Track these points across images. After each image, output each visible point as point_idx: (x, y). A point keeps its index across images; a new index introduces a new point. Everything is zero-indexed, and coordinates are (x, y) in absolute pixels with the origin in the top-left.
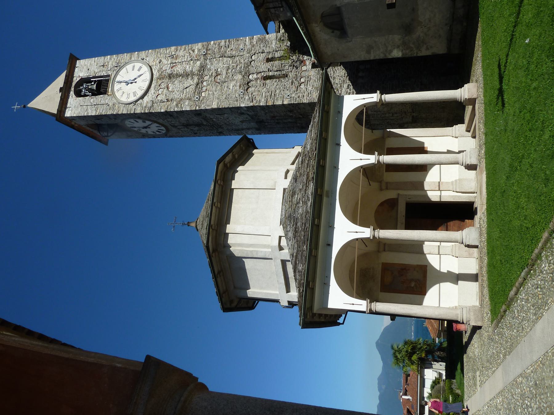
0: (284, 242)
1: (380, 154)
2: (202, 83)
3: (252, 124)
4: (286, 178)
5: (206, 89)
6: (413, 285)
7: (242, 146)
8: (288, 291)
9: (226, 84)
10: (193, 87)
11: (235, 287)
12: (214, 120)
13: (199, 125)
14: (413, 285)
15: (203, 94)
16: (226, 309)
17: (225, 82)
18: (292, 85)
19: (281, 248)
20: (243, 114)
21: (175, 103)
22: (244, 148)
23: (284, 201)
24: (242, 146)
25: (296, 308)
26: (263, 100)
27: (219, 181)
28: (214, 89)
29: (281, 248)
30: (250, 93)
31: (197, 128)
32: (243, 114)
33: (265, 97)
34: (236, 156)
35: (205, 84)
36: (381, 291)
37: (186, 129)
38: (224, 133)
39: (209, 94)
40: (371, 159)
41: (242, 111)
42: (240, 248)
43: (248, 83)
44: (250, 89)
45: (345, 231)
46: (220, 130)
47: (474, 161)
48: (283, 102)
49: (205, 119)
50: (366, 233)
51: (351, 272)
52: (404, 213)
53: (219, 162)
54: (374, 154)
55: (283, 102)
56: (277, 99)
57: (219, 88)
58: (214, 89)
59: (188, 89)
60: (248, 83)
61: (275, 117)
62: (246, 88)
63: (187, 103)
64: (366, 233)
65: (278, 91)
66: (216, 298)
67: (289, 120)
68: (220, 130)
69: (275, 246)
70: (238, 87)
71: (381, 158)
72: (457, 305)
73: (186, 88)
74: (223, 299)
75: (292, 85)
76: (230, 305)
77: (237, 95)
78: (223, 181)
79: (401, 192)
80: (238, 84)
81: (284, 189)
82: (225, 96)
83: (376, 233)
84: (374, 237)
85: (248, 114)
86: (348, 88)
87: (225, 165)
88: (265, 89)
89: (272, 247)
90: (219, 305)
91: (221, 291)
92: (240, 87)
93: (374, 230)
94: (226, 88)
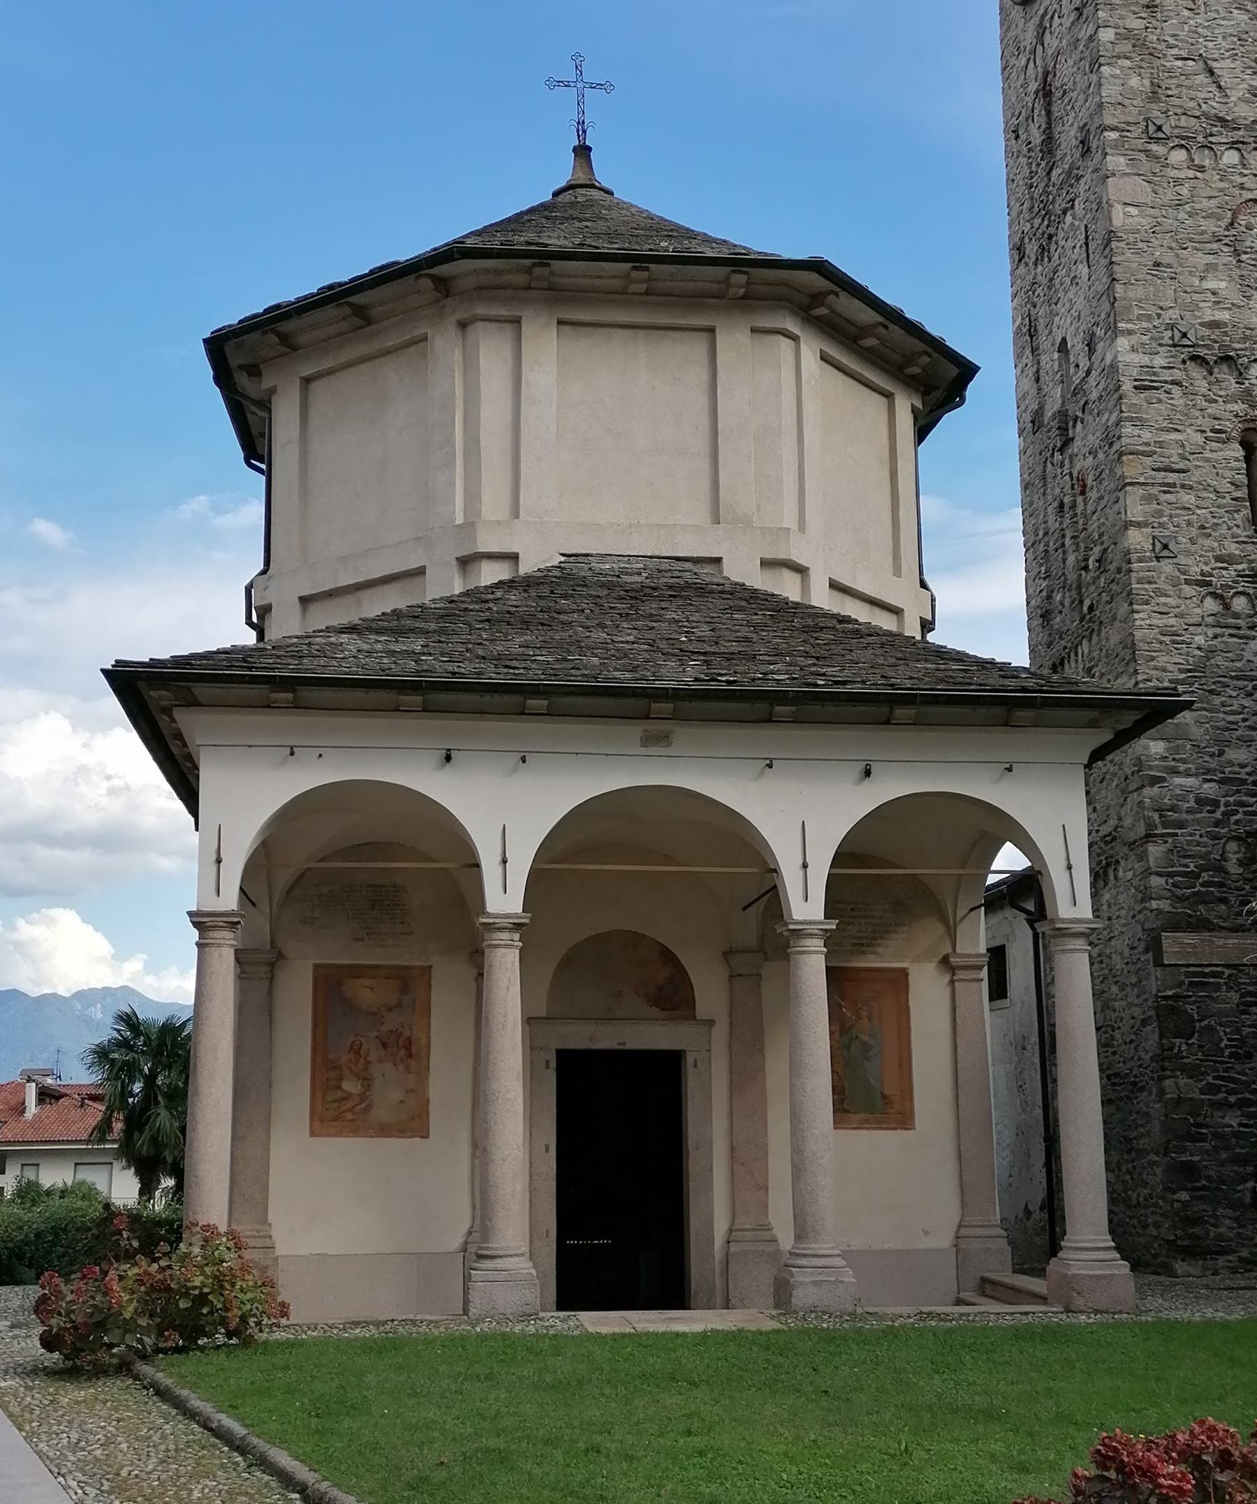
0: (490, 574)
1: (830, 940)
2: (1233, 145)
3: (1058, 392)
4: (766, 564)
5: (1201, 168)
6: (351, 1086)
7: (925, 360)
8: (834, 586)
9: (1226, 258)
10: (1216, 107)
11: (307, 381)
12: (1069, 219)
13: (1049, 143)
14: (351, 1086)
15: (1179, 156)
16: (219, 347)
17: (1237, 253)
18: (1218, 559)
19: (466, 562)
20: (1091, 346)
21: (1136, 24)
22: (915, 370)
23: (665, 565)
24: (925, 360)
25: (249, 638)
26: (1146, 435)
27: (741, 279)
28: (1206, 204)
29: (466, 562)
30: (1178, 374)
31: (1037, 137)
32: (1091, 346)
33: (1161, 444)
34: (870, 342)
35: (1231, 157)
36: (316, 967)
37: (1033, 86)
38: (1022, 270)
39: (1178, 182)
40: (806, 904)
41: (1100, 347)
42: (459, 391)
43: (1227, 359)
44: (1197, 372)
45: (506, 811)
46: (1031, 249)
47: (803, 1296)
48: (1138, 525)
49: (1072, 177)
50: (504, 896)
51: (381, 849)
52: (632, 1045)
53: (819, 267)
54: (827, 916)
55: (1138, 525)
56: (1148, 499)
57: (1210, 226)
58: (1206, 204)
59: (1202, 79)
60: (1227, 359)
61: (1083, 493)
62: (1202, 352)
63: (1134, 81)
64: (504, 896)
65: (1188, 498)
66: (257, 306)
67: (1071, 559)
68: (1031, 249)
69: (474, 541)
70: (1209, 315)
71: (817, 945)
72: (278, 1252)
73: (1211, 72)
74: (255, 336)
75: (1218, 559)
76: (241, 367)
77: (1173, 315)
78: (745, 297)
79: (720, 1034)
80: (1225, 316)
81: (718, 561)
82: (1168, 258)
83: (505, 935)
84: (489, 927)
85: (1088, 372)
86: (1199, 801)
87: (818, 298)
88: (1199, 438)
89: (469, 527)
90: (232, 318)
91: (286, 326)
92: (1214, 325)
93: (518, 927)
94: (1210, 259)
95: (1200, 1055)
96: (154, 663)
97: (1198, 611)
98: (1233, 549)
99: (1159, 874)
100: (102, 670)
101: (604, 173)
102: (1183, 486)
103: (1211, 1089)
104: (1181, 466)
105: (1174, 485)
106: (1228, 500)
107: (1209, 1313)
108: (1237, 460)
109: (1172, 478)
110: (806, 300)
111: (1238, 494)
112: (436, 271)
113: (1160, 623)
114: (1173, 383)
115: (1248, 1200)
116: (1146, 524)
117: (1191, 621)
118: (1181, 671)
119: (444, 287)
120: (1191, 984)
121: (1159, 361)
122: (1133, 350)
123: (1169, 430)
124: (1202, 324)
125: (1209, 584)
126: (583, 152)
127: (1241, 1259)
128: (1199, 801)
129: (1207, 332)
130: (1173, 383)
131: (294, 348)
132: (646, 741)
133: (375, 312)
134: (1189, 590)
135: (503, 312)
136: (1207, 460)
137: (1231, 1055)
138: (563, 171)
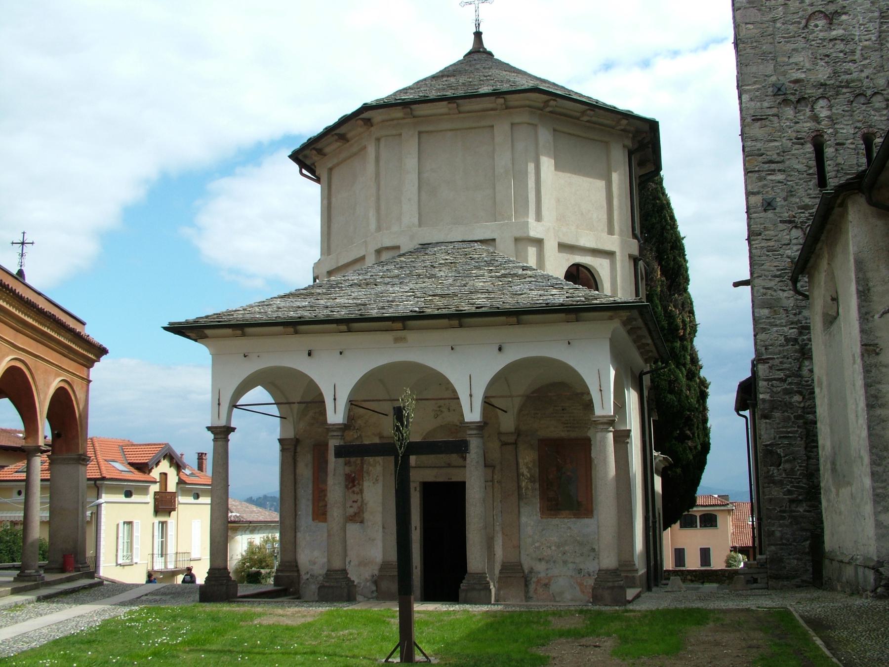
9: (801, 43)
92: (797, 81)
95: (784, 475)
96: (187, 322)
97: (788, 237)
98: (807, 201)
99: (765, 380)
100: (165, 328)
101: (488, 45)
102: (779, 170)
103: (789, 492)
104: (778, 159)
105: (774, 170)
106: (805, 175)
107: (723, 604)
108: (810, 153)
109: (773, 166)
110: (542, 105)
111: (811, 171)
112: (362, 116)
113: (766, 245)
114: (773, 115)
115: (807, 550)
116: (758, 193)
117: (783, 243)
118: (778, 270)
119: (368, 122)
120: (780, 437)
121: (766, 104)
122: (751, 100)
123: (771, 141)
124: (790, 82)
125: (793, 222)
126: (478, 35)
127: (803, 581)
128: (787, 340)
129: (792, 85)
130: (773, 115)
131: (325, 155)
132: (397, 340)
133: (349, 136)
134: (782, 226)
135: (394, 132)
136: (793, 155)
137: (800, 474)
138: (468, 45)
